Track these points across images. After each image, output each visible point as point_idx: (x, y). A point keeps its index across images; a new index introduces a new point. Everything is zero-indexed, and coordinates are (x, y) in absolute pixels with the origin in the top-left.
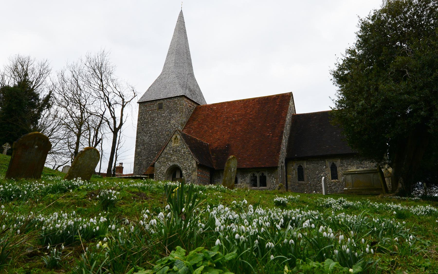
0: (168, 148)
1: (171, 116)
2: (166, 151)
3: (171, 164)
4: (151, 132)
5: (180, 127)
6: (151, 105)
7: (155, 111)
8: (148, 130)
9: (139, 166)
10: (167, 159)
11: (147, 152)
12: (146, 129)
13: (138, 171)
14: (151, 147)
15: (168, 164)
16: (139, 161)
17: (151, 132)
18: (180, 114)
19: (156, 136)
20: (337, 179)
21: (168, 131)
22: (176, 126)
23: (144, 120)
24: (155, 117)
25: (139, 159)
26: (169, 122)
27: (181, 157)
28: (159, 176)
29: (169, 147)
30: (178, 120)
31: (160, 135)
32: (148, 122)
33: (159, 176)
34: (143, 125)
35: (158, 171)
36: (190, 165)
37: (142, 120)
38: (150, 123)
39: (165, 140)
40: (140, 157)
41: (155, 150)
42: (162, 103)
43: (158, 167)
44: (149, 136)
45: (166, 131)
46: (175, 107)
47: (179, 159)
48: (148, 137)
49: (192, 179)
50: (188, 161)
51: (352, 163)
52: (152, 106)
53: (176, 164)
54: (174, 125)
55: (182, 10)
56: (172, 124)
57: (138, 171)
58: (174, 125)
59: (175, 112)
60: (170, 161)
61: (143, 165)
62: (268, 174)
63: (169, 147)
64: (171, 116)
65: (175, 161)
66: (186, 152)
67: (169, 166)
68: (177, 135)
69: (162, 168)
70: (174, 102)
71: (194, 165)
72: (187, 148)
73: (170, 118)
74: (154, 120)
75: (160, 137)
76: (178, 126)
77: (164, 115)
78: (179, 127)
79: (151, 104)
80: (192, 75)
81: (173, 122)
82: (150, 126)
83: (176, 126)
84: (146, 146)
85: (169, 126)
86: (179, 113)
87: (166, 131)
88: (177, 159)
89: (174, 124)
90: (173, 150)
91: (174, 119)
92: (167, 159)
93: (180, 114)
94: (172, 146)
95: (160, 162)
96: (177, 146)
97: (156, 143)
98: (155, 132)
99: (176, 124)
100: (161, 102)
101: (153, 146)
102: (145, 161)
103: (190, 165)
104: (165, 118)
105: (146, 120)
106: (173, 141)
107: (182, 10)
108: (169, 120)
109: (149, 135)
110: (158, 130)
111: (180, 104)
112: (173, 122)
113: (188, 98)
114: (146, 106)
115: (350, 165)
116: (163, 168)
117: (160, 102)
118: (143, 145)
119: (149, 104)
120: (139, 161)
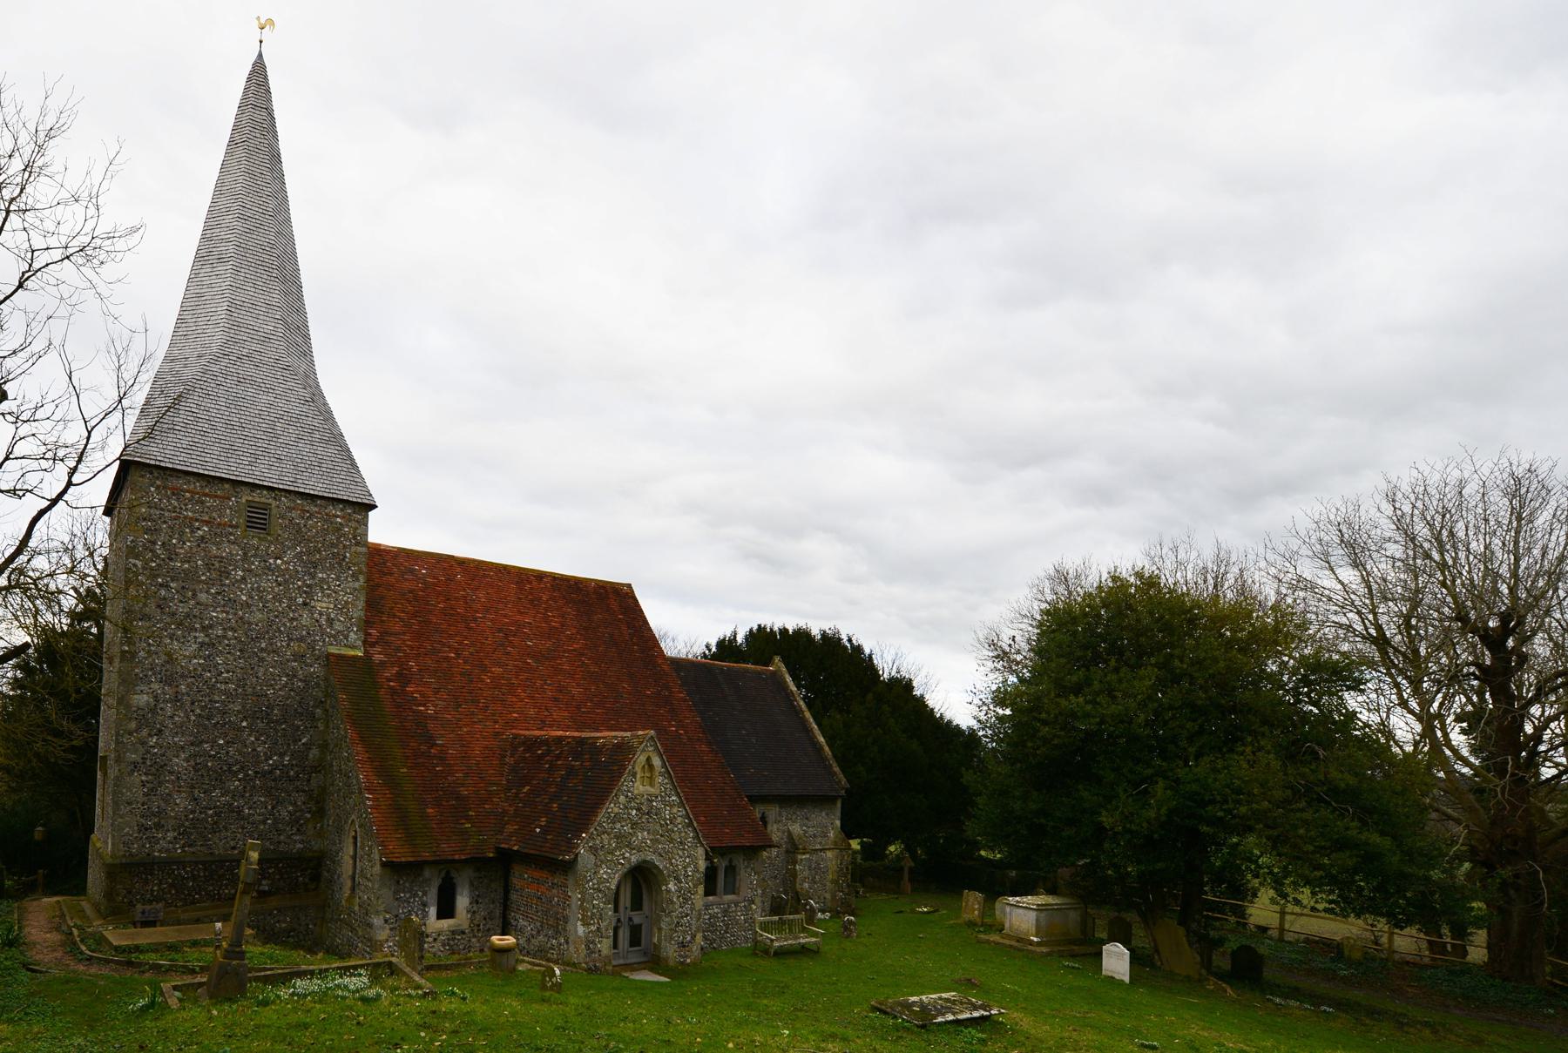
0: (622, 799)
1: (313, 577)
2: (616, 810)
3: (634, 859)
5: (356, 633)
7: (231, 534)
10: (618, 837)
11: (193, 718)
13: (141, 799)
14: (217, 698)
15: (624, 858)
17: (211, 627)
18: (358, 580)
19: (241, 651)
20: (912, 891)
21: (301, 639)
22: (338, 626)
23: (171, 559)
24: (230, 559)
25: (143, 743)
26: (305, 604)
28: (595, 902)
29: (627, 796)
31: (262, 650)
33: (595, 902)
34: (165, 586)
36: (689, 864)
37: (158, 557)
38: (202, 581)
39: (288, 675)
40: (150, 735)
45: (291, 640)
46: (333, 545)
47: (657, 840)
50: (684, 849)
53: (648, 858)
54: (330, 621)
55: (260, 55)
56: (321, 614)
57: (141, 799)
58: (330, 621)
60: (627, 846)
61: (171, 773)
62: (744, 860)
63: (627, 796)
64: (313, 577)
65: (643, 847)
66: (679, 820)
67: (627, 866)
69: (603, 871)
70: (325, 521)
71: (700, 862)
72: (682, 805)
76: (349, 630)
78: (352, 635)
80: (316, 398)
81: (324, 605)
82: (203, 597)
83: (338, 626)
84: (188, 686)
85: (305, 619)
86: (353, 576)
87: (291, 640)
88: (651, 840)
90: (638, 809)
91: (329, 596)
92: (618, 837)
93: (358, 580)
95: (596, 850)
96: (650, 795)
97: (241, 683)
98: (232, 629)
101: (227, 693)
103: (689, 864)
104: (286, 581)
106: (638, 776)
107: (260, 55)
108: (305, 592)
109: (201, 637)
110: (250, 624)
111: (355, 538)
116: (605, 872)
117: (256, 497)
118: (169, 680)
120: (148, 752)
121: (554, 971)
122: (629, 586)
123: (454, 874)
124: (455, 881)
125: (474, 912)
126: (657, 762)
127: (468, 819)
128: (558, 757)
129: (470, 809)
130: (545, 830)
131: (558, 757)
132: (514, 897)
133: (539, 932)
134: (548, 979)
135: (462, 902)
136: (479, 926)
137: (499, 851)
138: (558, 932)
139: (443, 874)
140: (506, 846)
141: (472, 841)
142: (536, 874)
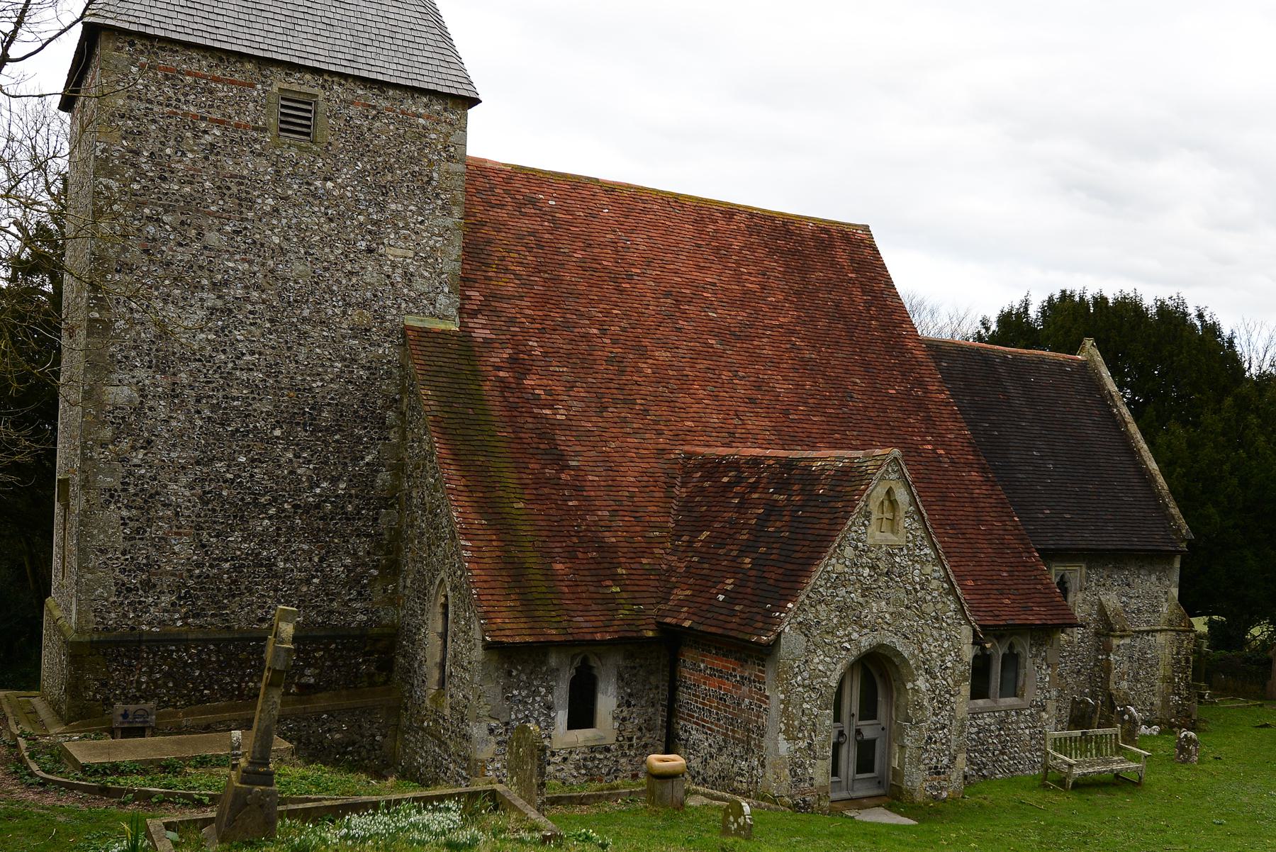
4: (226, 283)
6: (217, 80)
7: (255, 140)
8: (202, 260)
9: (128, 507)
11: (199, 423)
12: (183, 255)
13: (121, 545)
14: (235, 393)
16: (130, 473)
18: (450, 214)
19: (271, 321)
21: (364, 304)
22: (420, 285)
23: (164, 179)
27: (907, 608)
28: (805, 706)
30: (433, 249)
32: (193, 205)
33: (805, 706)
35: (796, 675)
36: (948, 651)
41: (269, 414)
42: (310, 100)
43: (797, 652)
44: (213, 310)
48: (201, 313)
49: (954, 717)
51: (1109, 582)
52: (222, 90)
53: (887, 641)
54: (408, 277)
56: (394, 266)
57: (121, 545)
58: (408, 277)
59: (411, 192)
63: (856, 548)
64: (382, 208)
66: (935, 584)
67: (855, 652)
68: (893, 484)
73: (375, 223)
74: (245, 201)
75: (305, 335)
77: (328, 192)
79: (218, 73)
81: (399, 252)
82: (212, 238)
85: (371, 274)
89: (405, 268)
93: (450, 214)
94: (870, 541)
97: (272, 371)
99: (422, 276)
100: (305, 89)
102: (184, 480)
103: (948, 651)
105: (181, 183)
109: (211, 299)
112: (396, 251)
113: (346, 76)
114: (172, 76)
115: (1104, 585)
118: (161, 365)
119: (203, 65)
121: (741, 807)
122: (866, 228)
123: (594, 662)
124: (595, 672)
125: (624, 719)
126: (902, 496)
127: (616, 579)
128: (754, 488)
129: (620, 565)
130: (732, 598)
131: (754, 488)
132: (683, 696)
133: (720, 749)
134: (732, 819)
135: (607, 702)
136: (630, 739)
137: (661, 627)
138: (748, 750)
139: (577, 662)
140: (674, 621)
141: (622, 613)
142: (719, 664)
